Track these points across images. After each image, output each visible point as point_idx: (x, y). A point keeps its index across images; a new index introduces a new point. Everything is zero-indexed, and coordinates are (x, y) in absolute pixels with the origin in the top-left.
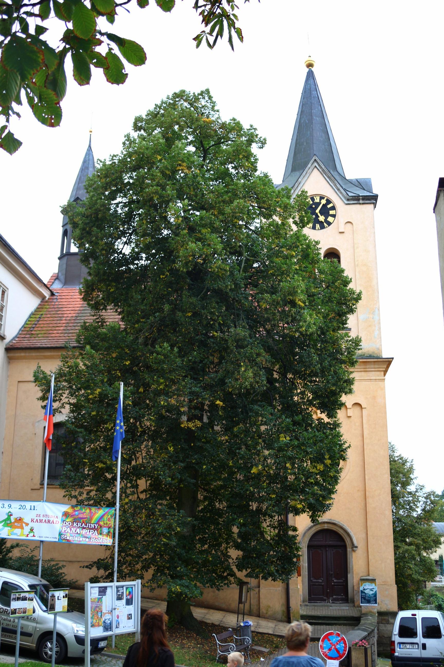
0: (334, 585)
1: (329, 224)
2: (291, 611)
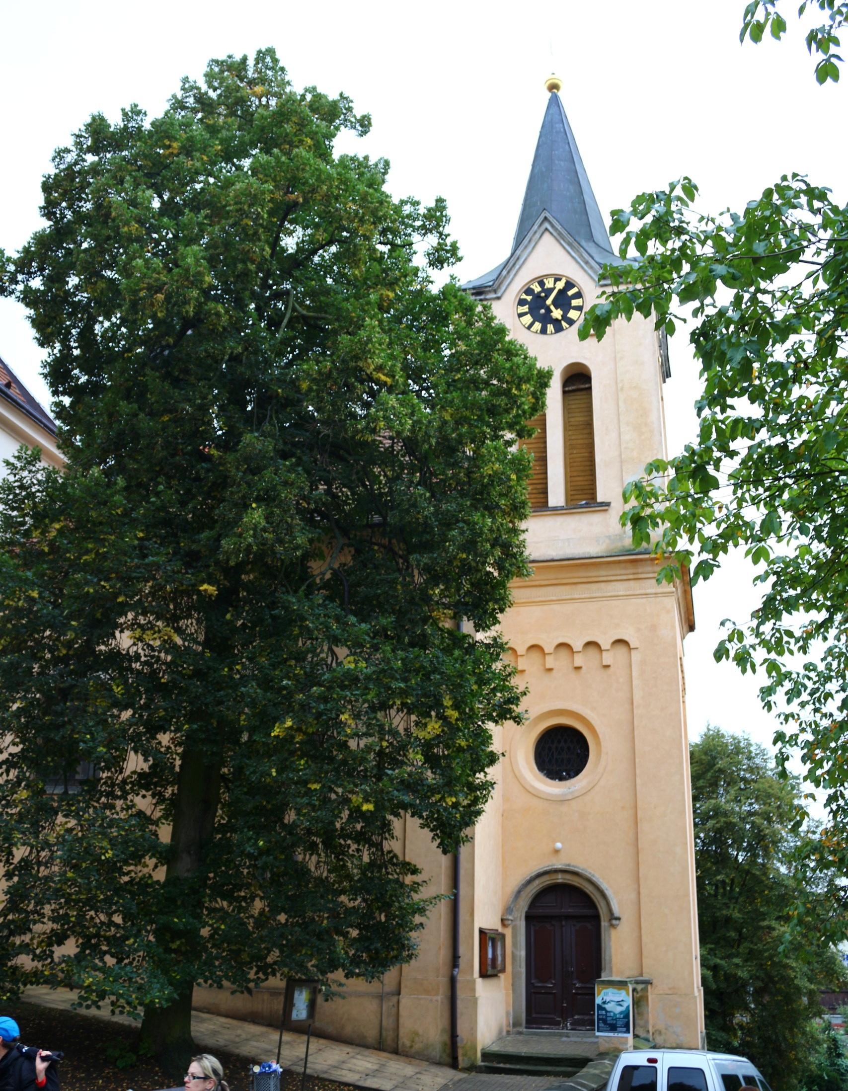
0: (576, 994)
2: (459, 1045)
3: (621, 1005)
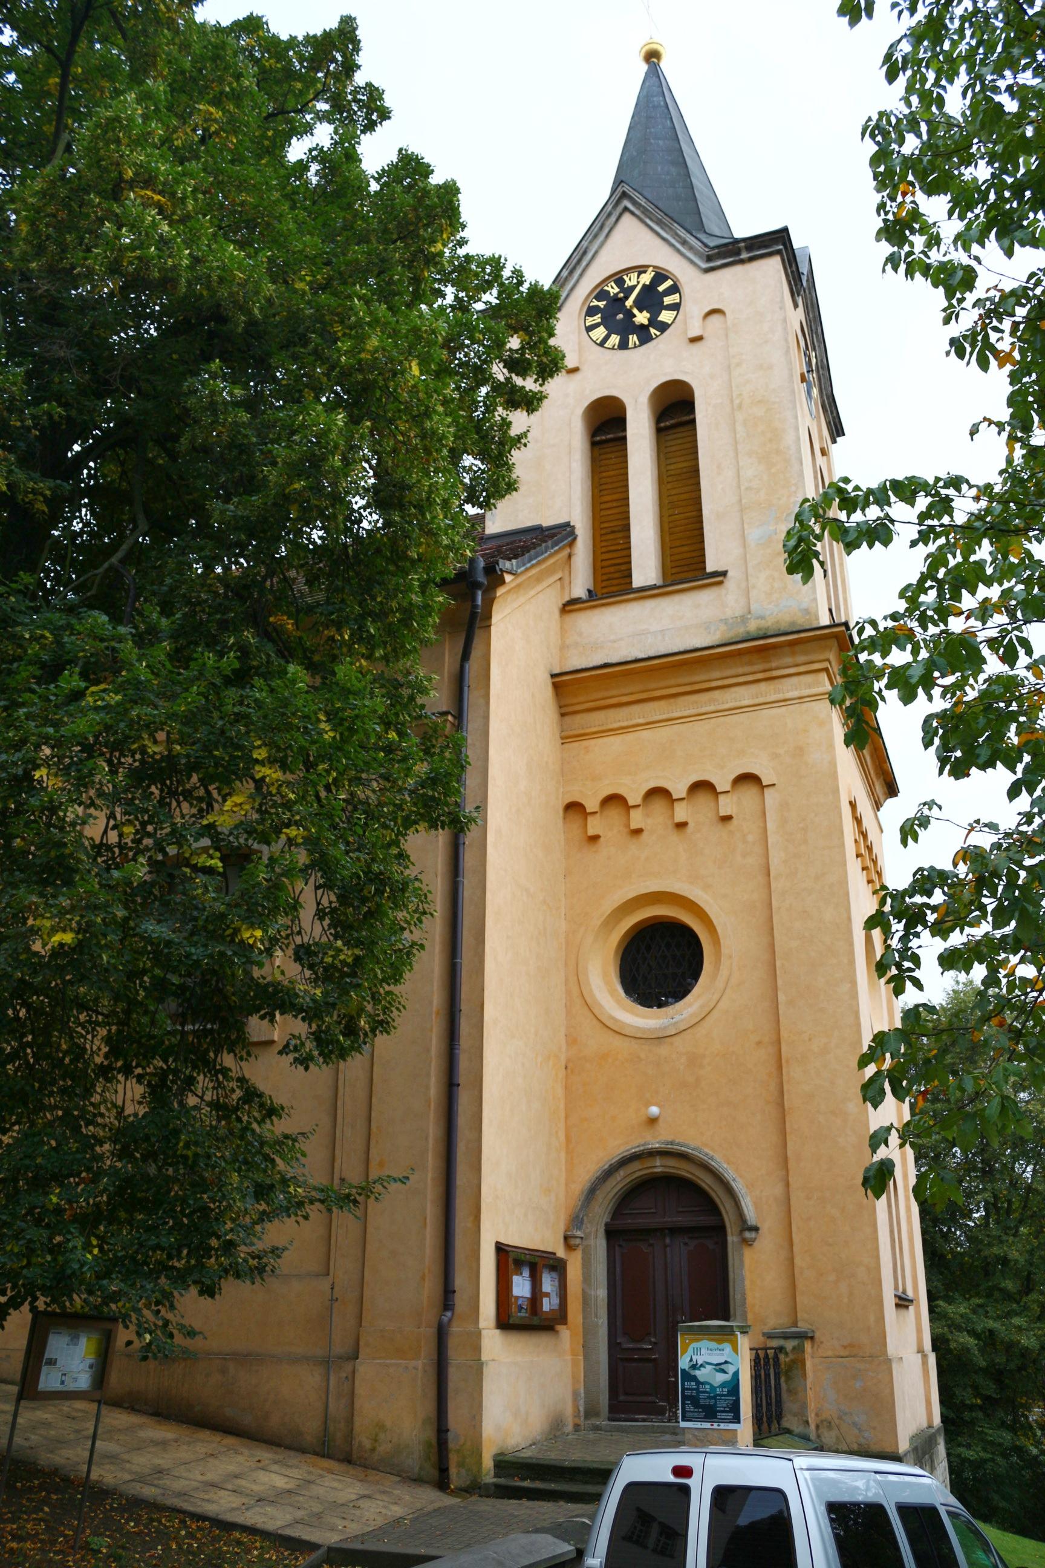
1: (663, 327)
2: (451, 1445)
3: (724, 1372)
